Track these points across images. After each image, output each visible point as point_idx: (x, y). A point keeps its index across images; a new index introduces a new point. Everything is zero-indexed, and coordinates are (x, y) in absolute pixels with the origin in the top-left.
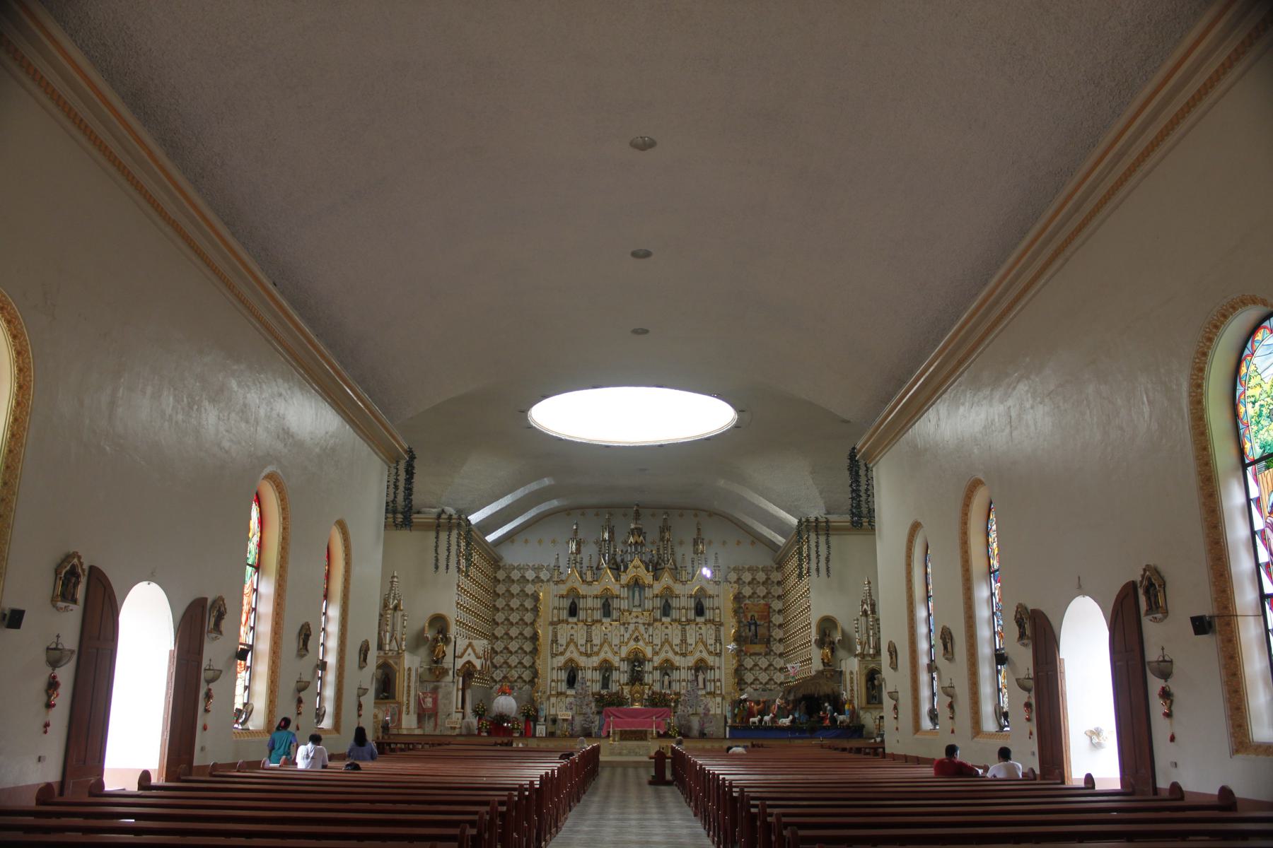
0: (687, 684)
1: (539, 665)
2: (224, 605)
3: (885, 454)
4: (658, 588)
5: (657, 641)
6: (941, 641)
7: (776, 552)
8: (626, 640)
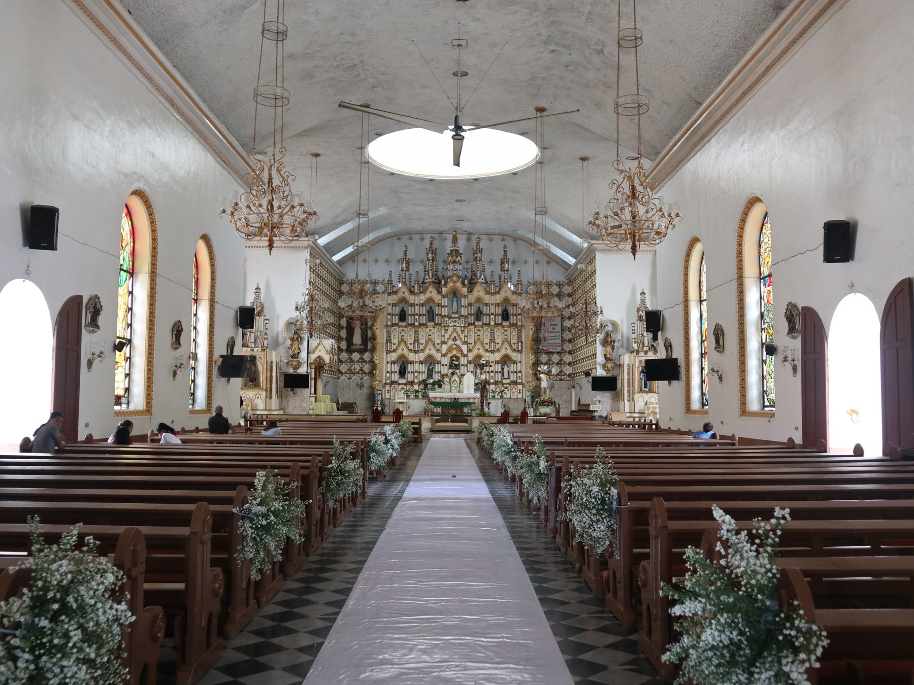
0: (495, 375)
1: (377, 359)
2: (100, 302)
3: (663, 186)
4: (472, 298)
5: (471, 341)
6: (713, 336)
7: (567, 270)
8: (446, 340)
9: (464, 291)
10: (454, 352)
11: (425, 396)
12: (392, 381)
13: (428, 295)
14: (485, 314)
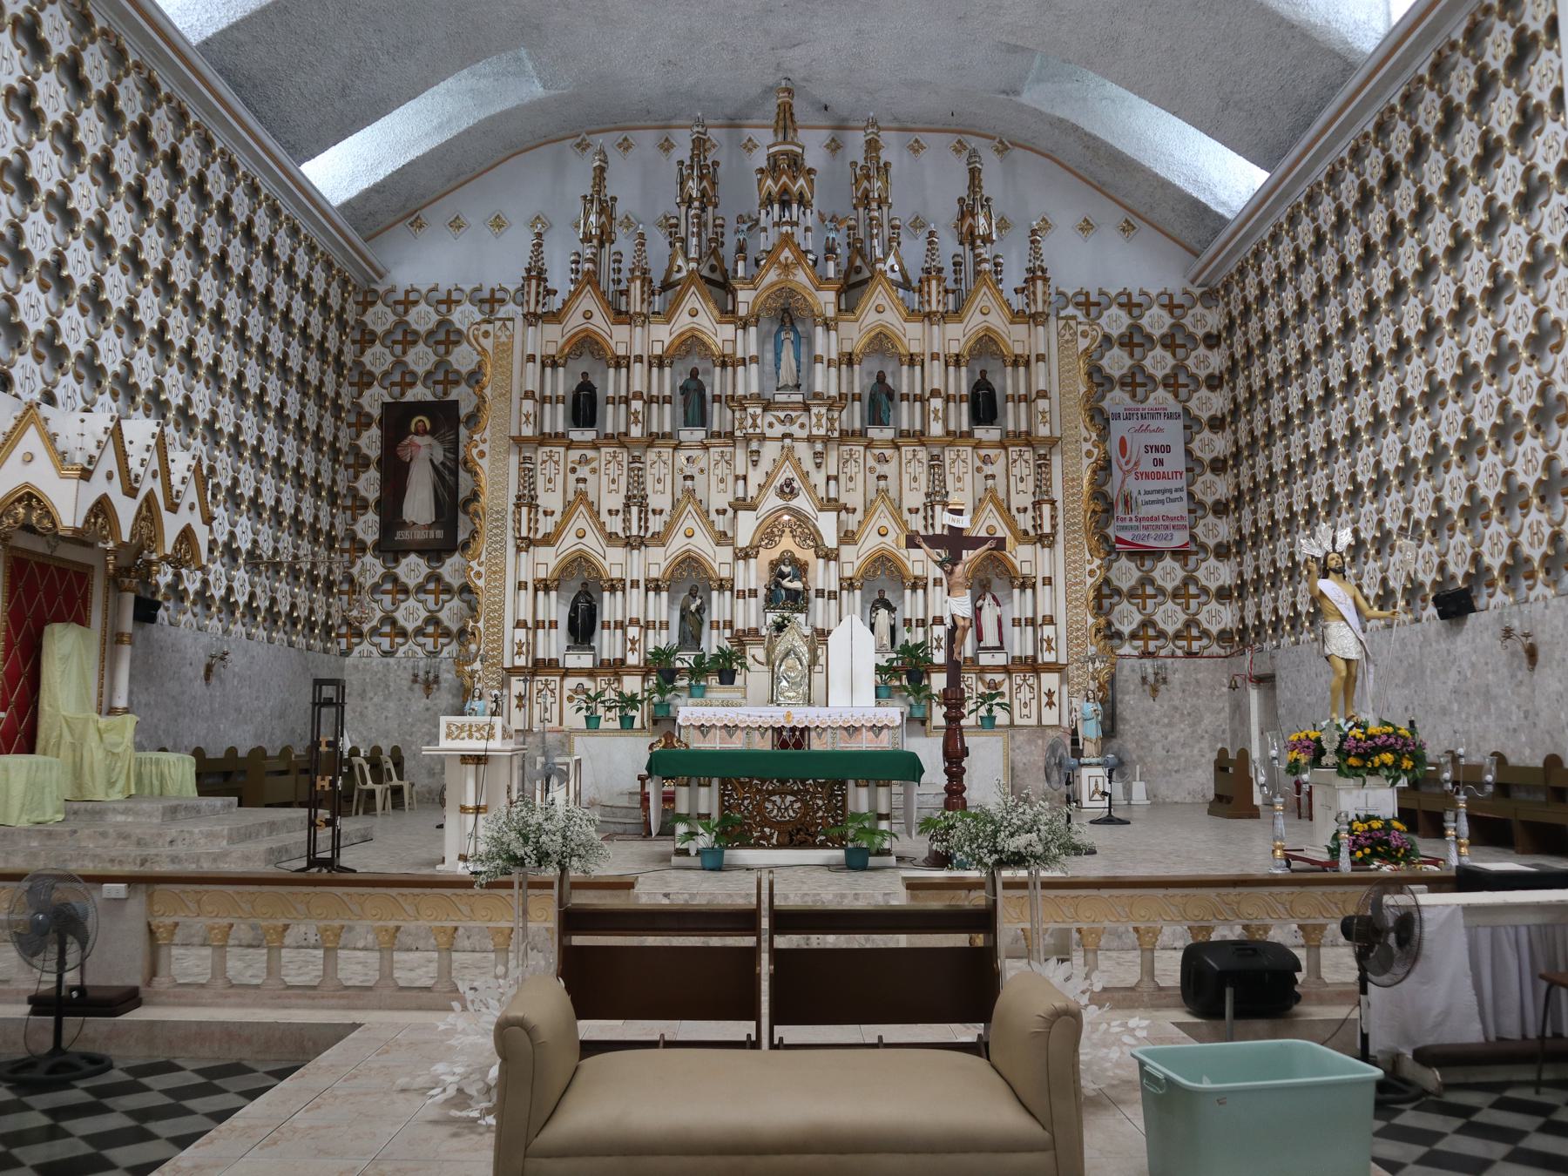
4: (854, 334)
7: (1197, 256)
8: (752, 491)
9: (826, 301)
10: (787, 543)
11: (663, 720)
12: (536, 662)
13: (683, 321)
14: (904, 397)
